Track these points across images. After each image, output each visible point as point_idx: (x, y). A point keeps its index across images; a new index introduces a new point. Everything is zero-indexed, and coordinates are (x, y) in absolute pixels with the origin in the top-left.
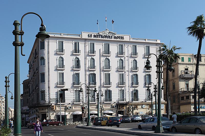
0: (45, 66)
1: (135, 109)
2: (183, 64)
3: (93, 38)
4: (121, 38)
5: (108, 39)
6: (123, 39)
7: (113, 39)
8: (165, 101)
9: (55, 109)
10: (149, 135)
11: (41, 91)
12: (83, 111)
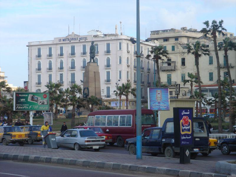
3: (62, 42)
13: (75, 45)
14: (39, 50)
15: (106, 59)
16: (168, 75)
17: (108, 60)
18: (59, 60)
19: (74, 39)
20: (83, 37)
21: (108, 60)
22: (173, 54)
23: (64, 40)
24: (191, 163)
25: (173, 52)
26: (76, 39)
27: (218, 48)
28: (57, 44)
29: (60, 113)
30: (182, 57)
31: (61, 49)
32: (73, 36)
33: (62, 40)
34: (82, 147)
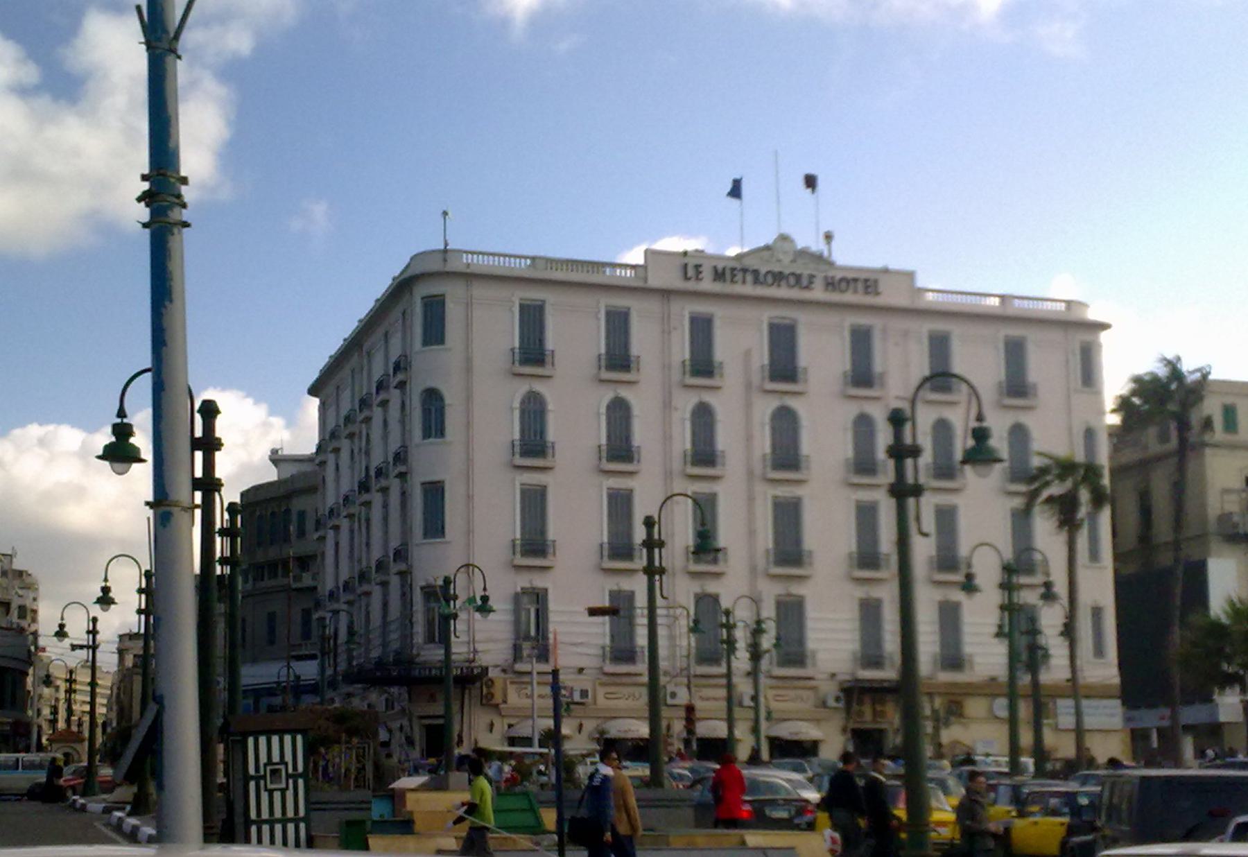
0: (186, 225)
1: (947, 724)
2: (1234, 447)
3: (707, 284)
4: (867, 287)
5: (795, 294)
6: (877, 294)
7: (818, 293)
8: (1114, 419)
9: (498, 698)
10: (390, 290)
11: (422, 588)
12: (654, 718)
13: (720, 314)
14: (532, 318)
15: (517, 404)
18: (686, 403)
23: (719, 275)
24: (418, 834)
28: (666, 294)
31: (702, 329)
32: (786, 260)
34: (219, 818)
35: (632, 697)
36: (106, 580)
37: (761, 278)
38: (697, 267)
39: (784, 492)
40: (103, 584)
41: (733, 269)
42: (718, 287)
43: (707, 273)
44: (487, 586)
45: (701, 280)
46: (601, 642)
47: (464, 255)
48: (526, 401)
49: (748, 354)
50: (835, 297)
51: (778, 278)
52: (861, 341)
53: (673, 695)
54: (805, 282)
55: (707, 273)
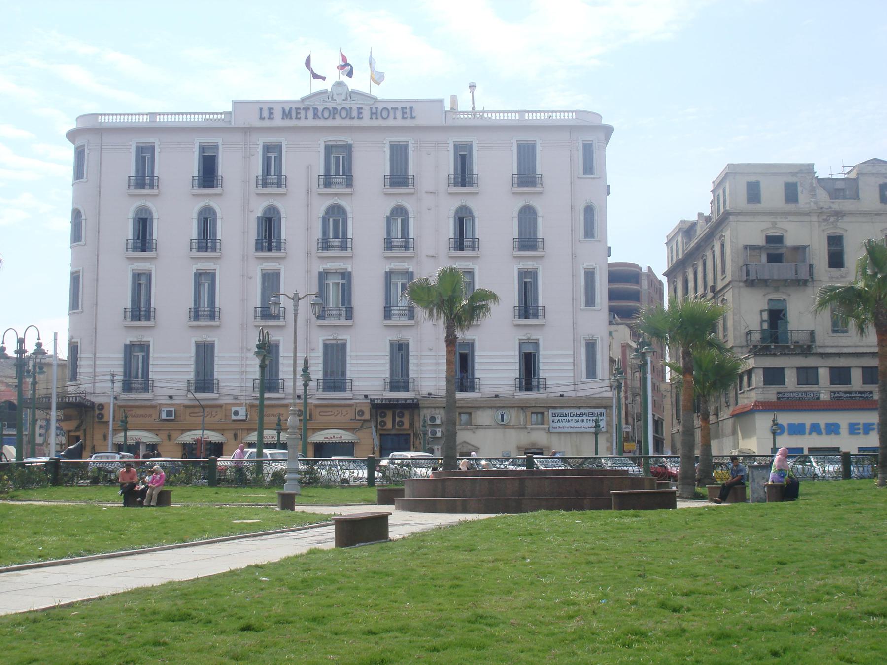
3: (278, 121)
5: (347, 123)
6: (412, 118)
7: (366, 121)
16: (770, 300)
17: (528, 216)
19: (344, 114)
20: (389, 106)
21: (528, 216)
22: (790, 218)
23: (286, 115)
25: (791, 207)
26: (355, 114)
27: (38, 370)
28: (247, 130)
29: (173, 409)
30: (832, 231)
33: (278, 114)
35: (210, 416)
36: (39, 339)
37: (320, 114)
38: (270, 110)
39: (270, 266)
40: (38, 341)
41: (297, 109)
42: (288, 123)
43: (278, 114)
44: (40, 336)
45: (362, 118)
46: (384, 376)
47: (527, 114)
48: (395, 212)
49: (309, 167)
50: (380, 122)
51: (334, 113)
52: (399, 154)
53: (236, 413)
54: (355, 114)
55: (366, 114)
